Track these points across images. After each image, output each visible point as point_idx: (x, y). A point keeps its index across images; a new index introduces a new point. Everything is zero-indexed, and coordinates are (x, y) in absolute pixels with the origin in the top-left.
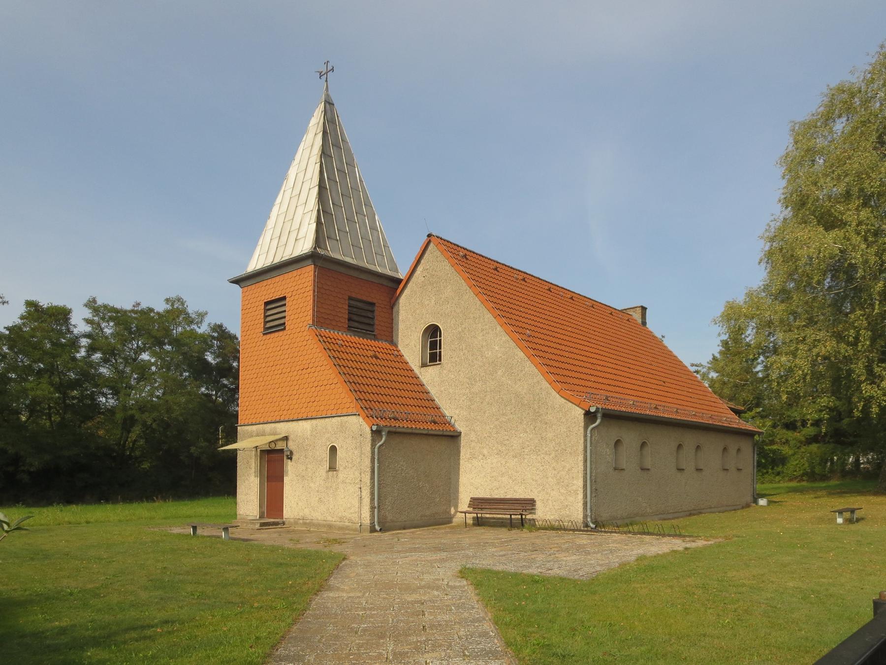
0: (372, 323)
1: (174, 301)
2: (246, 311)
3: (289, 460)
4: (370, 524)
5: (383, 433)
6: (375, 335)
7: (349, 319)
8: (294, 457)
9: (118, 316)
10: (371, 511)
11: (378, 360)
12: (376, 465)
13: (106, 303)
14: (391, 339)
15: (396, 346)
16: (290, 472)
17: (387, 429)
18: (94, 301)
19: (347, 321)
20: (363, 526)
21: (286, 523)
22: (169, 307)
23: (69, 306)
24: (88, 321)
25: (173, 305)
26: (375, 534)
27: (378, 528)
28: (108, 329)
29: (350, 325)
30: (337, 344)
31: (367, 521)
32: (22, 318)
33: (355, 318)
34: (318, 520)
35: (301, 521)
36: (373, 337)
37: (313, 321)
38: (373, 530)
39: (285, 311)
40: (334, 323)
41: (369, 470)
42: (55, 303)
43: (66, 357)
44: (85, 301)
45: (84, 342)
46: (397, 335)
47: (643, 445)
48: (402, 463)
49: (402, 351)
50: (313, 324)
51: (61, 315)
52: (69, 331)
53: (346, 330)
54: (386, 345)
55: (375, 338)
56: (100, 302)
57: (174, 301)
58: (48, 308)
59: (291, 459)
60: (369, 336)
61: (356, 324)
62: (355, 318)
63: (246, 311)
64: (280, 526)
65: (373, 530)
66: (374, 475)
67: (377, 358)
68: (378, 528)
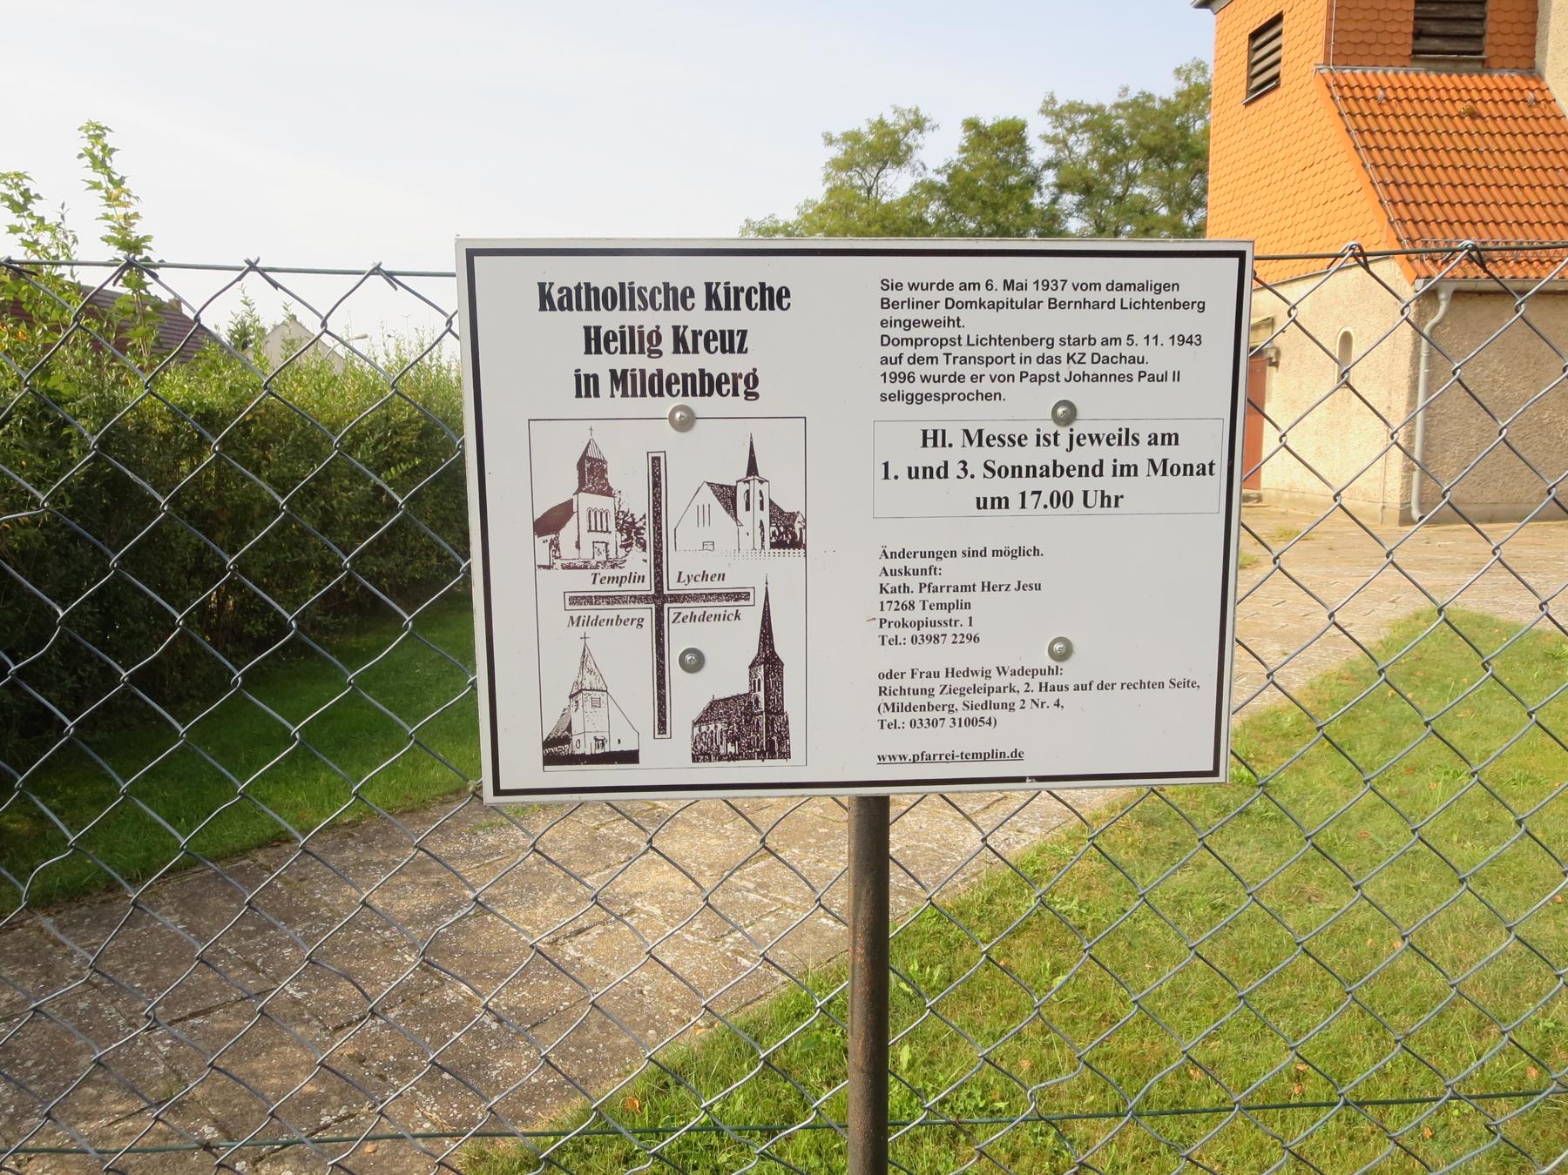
0: (1478, 32)
1: (1190, 71)
2: (1222, 62)
3: (1274, 368)
4: (1402, 505)
5: (1442, 296)
6: (1483, 61)
7: (1418, 35)
8: (1282, 362)
9: (1098, 124)
10: (1403, 478)
11: (1478, 122)
12: (1423, 371)
13: (1072, 99)
14: (1529, 67)
15: (1539, 78)
16: (1274, 394)
17: (1453, 286)
18: (1053, 100)
19: (1410, 40)
20: (1386, 510)
21: (1264, 498)
22: (1183, 86)
23: (1021, 117)
24: (1051, 140)
25: (1187, 79)
26: (1411, 529)
27: (1416, 514)
28: (1081, 146)
29: (1417, 48)
30: (1524, 100)
31: (1395, 500)
32: (964, 150)
33: (1434, 28)
34: (1313, 493)
35: (1287, 496)
36: (1479, 66)
37: (1327, 54)
38: (1406, 519)
39: (1279, 48)
40: (1362, 50)
41: (1405, 383)
42: (1002, 117)
43: (1015, 206)
44: (1040, 105)
45: (1049, 177)
46: (1545, 50)
47: (1362, 258)
48: (1494, 365)
49: (1553, 89)
50: (1326, 63)
51: (1012, 135)
52: (1024, 162)
53: (1407, 62)
54: (1512, 79)
55: (1486, 66)
56: (1061, 101)
57: (1190, 71)
58: (993, 127)
59: (1276, 364)
60: (1465, 66)
61: (1435, 43)
62: (1434, 28)
63: (1222, 62)
64: (1250, 504)
65: (1406, 519)
66: (1417, 393)
67: (1474, 115)
68: (1416, 514)
